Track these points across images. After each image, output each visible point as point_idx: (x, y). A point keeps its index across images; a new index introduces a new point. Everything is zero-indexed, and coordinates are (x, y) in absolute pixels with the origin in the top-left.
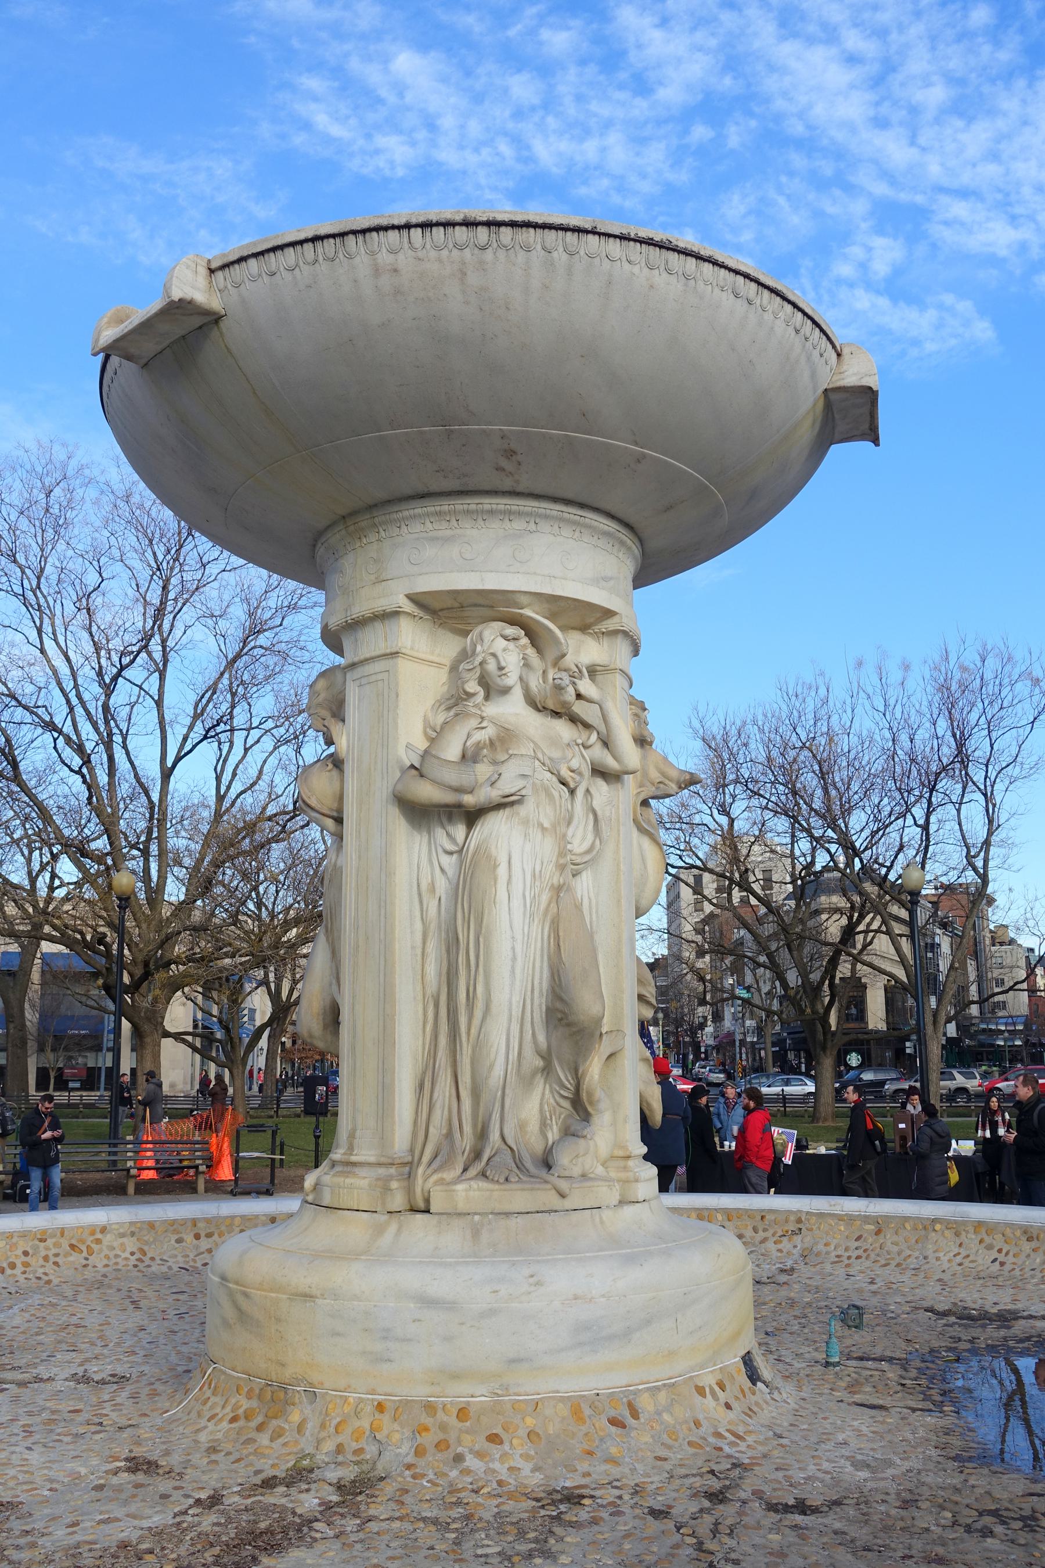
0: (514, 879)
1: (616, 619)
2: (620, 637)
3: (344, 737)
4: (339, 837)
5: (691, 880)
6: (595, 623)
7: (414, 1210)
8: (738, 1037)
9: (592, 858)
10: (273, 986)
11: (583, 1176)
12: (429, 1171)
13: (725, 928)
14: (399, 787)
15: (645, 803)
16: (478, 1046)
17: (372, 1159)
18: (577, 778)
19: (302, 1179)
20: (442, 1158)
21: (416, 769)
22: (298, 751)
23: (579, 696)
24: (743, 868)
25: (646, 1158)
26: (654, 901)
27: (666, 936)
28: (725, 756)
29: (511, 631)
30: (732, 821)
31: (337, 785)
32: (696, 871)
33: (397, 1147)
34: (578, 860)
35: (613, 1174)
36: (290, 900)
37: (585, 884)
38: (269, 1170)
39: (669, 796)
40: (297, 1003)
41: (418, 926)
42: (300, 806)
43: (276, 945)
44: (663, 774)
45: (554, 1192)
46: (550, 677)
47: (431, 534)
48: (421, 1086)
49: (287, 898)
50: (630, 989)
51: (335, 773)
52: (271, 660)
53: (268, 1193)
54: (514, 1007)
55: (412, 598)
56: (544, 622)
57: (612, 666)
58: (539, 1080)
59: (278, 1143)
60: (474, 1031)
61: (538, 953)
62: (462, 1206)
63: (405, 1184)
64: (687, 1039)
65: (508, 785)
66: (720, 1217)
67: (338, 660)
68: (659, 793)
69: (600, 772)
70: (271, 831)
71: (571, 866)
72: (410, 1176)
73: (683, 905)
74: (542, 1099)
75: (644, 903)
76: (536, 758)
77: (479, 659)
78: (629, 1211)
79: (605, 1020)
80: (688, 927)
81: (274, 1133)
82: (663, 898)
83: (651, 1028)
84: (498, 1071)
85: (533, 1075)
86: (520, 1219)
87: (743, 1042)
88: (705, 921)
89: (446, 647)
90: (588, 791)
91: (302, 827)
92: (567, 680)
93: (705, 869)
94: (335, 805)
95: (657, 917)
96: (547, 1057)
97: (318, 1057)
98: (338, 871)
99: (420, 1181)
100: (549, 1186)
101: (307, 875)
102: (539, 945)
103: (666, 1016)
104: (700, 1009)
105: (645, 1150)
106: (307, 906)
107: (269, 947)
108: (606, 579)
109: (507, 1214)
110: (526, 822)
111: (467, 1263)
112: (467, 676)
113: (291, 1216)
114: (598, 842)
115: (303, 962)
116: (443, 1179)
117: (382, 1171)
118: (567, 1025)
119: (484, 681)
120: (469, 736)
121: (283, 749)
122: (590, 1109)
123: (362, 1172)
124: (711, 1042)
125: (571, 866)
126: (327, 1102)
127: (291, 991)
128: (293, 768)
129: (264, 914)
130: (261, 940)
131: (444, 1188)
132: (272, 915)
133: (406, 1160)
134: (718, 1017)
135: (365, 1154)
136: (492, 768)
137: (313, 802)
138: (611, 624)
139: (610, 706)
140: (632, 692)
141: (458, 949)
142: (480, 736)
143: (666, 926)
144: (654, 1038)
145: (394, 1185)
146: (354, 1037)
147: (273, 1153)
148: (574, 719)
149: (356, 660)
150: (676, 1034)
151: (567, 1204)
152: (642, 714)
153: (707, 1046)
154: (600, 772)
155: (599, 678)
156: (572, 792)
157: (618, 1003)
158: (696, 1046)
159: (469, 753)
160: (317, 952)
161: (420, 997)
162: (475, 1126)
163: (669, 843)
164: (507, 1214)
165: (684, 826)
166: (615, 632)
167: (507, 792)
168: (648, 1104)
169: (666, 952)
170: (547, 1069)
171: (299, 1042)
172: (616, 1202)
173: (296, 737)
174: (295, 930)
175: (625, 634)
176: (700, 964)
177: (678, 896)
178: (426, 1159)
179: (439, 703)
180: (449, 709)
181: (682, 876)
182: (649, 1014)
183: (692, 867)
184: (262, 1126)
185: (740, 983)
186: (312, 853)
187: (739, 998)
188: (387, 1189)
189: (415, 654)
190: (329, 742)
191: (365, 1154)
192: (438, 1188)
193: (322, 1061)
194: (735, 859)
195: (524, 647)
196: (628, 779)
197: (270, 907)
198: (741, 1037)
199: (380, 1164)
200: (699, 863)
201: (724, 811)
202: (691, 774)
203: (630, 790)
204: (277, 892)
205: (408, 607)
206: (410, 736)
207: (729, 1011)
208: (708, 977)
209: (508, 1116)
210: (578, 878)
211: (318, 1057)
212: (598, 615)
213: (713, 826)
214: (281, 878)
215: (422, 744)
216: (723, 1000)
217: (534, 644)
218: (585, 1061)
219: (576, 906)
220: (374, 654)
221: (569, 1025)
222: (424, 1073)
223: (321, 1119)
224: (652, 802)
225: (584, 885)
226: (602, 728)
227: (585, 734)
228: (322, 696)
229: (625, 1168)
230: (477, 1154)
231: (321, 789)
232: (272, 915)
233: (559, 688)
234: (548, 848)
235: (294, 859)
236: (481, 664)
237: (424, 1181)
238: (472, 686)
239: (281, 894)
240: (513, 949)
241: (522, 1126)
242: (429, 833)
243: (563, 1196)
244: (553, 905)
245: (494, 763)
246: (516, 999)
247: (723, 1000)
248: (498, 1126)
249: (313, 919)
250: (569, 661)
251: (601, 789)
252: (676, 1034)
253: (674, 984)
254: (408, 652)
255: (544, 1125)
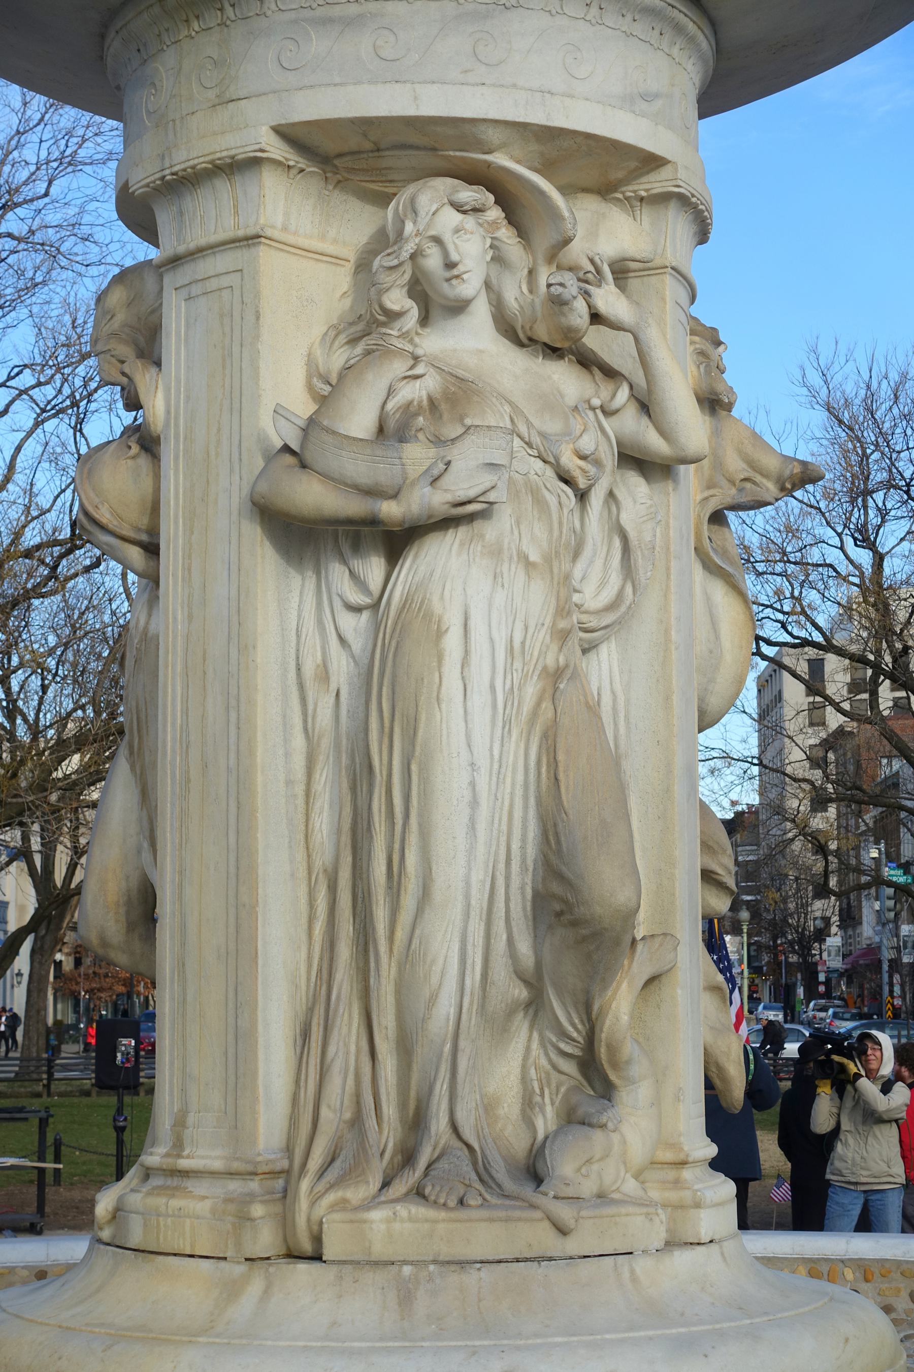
0: (474, 658)
1: (665, 173)
2: (673, 205)
3: (160, 395)
4: (152, 579)
5: (803, 668)
6: (626, 181)
7: (293, 1255)
8: (887, 955)
9: (618, 617)
10: (38, 860)
11: (601, 1196)
12: (321, 1187)
13: (864, 754)
14: (263, 487)
15: (718, 518)
16: (410, 959)
17: (217, 1165)
18: (592, 470)
19: (92, 1203)
20: (344, 1162)
21: (293, 452)
22: (78, 429)
23: (596, 318)
24: (898, 645)
25: (715, 1164)
26: (730, 704)
27: (755, 770)
28: (870, 436)
29: (469, 194)
30: (879, 560)
31: (147, 483)
32: (811, 652)
33: (261, 1144)
34: (593, 623)
35: (655, 1194)
36: (68, 705)
37: (605, 666)
38: (34, 1189)
39: (759, 504)
40: (78, 891)
41: (299, 742)
42: (83, 529)
43: (43, 785)
44: (752, 464)
45: (546, 1224)
46: (542, 281)
47: (320, 12)
48: (305, 1034)
49: (61, 699)
50: (687, 860)
51: (144, 461)
52: (28, 260)
53: (33, 1230)
54: (474, 892)
55: (284, 133)
56: (528, 177)
57: (658, 262)
58: (521, 1027)
59: (50, 1139)
60: (401, 934)
61: (519, 792)
62: (379, 1250)
63: (277, 1208)
64: (793, 958)
65: (463, 482)
66: (849, 1274)
67: (151, 253)
68: (743, 499)
69: (634, 460)
70: (30, 575)
71: (579, 634)
72: (286, 1195)
73: (788, 712)
74: (526, 1058)
75: (714, 702)
76: (515, 432)
77: (409, 248)
78: (682, 1259)
79: (641, 915)
80: (797, 755)
81: (43, 1123)
82: (749, 698)
83: (728, 938)
84: (446, 1007)
85: (510, 1014)
86: (486, 1273)
87: (895, 964)
88: (827, 744)
89: (350, 226)
90: (611, 494)
91: (87, 569)
92: (572, 287)
93: (829, 647)
94: (144, 522)
95: (738, 733)
96: (534, 982)
97: (121, 989)
98: (150, 642)
99: (303, 1203)
100: (538, 1214)
101: (99, 657)
102: (520, 777)
103: (756, 915)
104: (818, 904)
105: (712, 1150)
106: (97, 713)
107: (30, 788)
108: (647, 97)
109: (463, 1264)
110: (496, 552)
111: (390, 1351)
112: (386, 279)
113: (70, 1267)
114: (629, 589)
115: (90, 814)
116: (345, 1201)
117: (234, 1186)
118: (570, 926)
119: (419, 290)
120: (390, 392)
121: (49, 426)
122: (612, 1077)
123: (199, 1187)
124: (836, 963)
125: (579, 634)
126: (136, 1069)
127: (72, 868)
128: (69, 460)
129: (21, 731)
130: (15, 775)
131: (348, 1216)
132: (35, 731)
133: (278, 1167)
134: (850, 919)
135: (203, 1154)
136: (432, 452)
137: (104, 515)
138: (656, 182)
139: (653, 336)
140: (694, 311)
141: (371, 785)
142: (410, 392)
143: (755, 752)
144: (733, 957)
145: (258, 1210)
146: (183, 944)
147: (42, 1159)
148: (587, 361)
149: (182, 249)
150: (774, 950)
151: (572, 1246)
152: (714, 353)
153: (829, 971)
154: (634, 460)
155: (634, 283)
156: (582, 496)
157: (665, 887)
158: (810, 971)
159: (391, 424)
160: (117, 796)
161: (302, 872)
162: (403, 1105)
163: (763, 599)
164: (463, 1264)
165: (791, 568)
166: (664, 198)
167: (462, 494)
168: (720, 1068)
169: (755, 799)
170: (535, 1005)
171: (87, 961)
172: (659, 1244)
173: (75, 404)
174: (76, 758)
175: (683, 200)
176: (818, 823)
177: (779, 698)
178: (314, 1164)
179: (336, 330)
180: (353, 341)
181: (787, 661)
182: (721, 904)
183: (806, 643)
184: (21, 1110)
185: (892, 856)
186: (107, 618)
187: (890, 884)
188: (244, 1218)
189: (291, 239)
190: (133, 403)
191: (203, 1154)
192: (337, 1216)
193: (129, 995)
194: (884, 629)
195: (494, 224)
196: (687, 472)
197: (31, 717)
198: (892, 955)
199: (231, 1174)
200: (818, 637)
201: (866, 540)
202: (804, 464)
203: (689, 493)
204: (44, 688)
205: (277, 149)
206: (282, 391)
207: (870, 909)
208: (833, 846)
209: (464, 1089)
210: (592, 655)
211: (121, 989)
212: (633, 164)
213: (844, 567)
214: (52, 663)
215: (304, 408)
216: (860, 887)
217: (512, 219)
218: (605, 988)
219: (589, 707)
220: (214, 238)
221: (575, 924)
222: (311, 1010)
223: (127, 1099)
224: (731, 516)
225: (604, 669)
226: (639, 379)
227: (606, 388)
228: (120, 317)
229: (677, 1183)
230: (407, 1157)
231: (120, 489)
232: (35, 731)
233: (558, 303)
234: (536, 600)
235: (74, 630)
236: (413, 257)
237: (311, 1204)
238: (396, 298)
239: (50, 693)
240: (473, 784)
241: (489, 1107)
242: (318, 573)
243: (563, 1231)
244: (546, 705)
245: (438, 441)
246: (479, 876)
247: (860, 887)
248: (444, 1106)
249: (111, 731)
250: (577, 251)
251: (636, 490)
252: (774, 950)
253: (770, 857)
254: (276, 234)
255: (528, 1104)
